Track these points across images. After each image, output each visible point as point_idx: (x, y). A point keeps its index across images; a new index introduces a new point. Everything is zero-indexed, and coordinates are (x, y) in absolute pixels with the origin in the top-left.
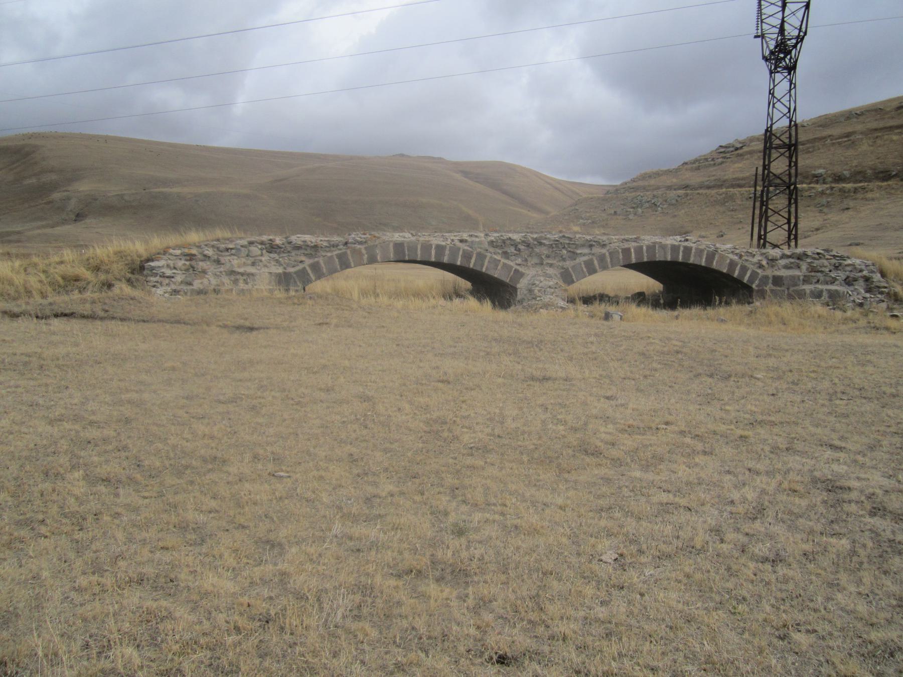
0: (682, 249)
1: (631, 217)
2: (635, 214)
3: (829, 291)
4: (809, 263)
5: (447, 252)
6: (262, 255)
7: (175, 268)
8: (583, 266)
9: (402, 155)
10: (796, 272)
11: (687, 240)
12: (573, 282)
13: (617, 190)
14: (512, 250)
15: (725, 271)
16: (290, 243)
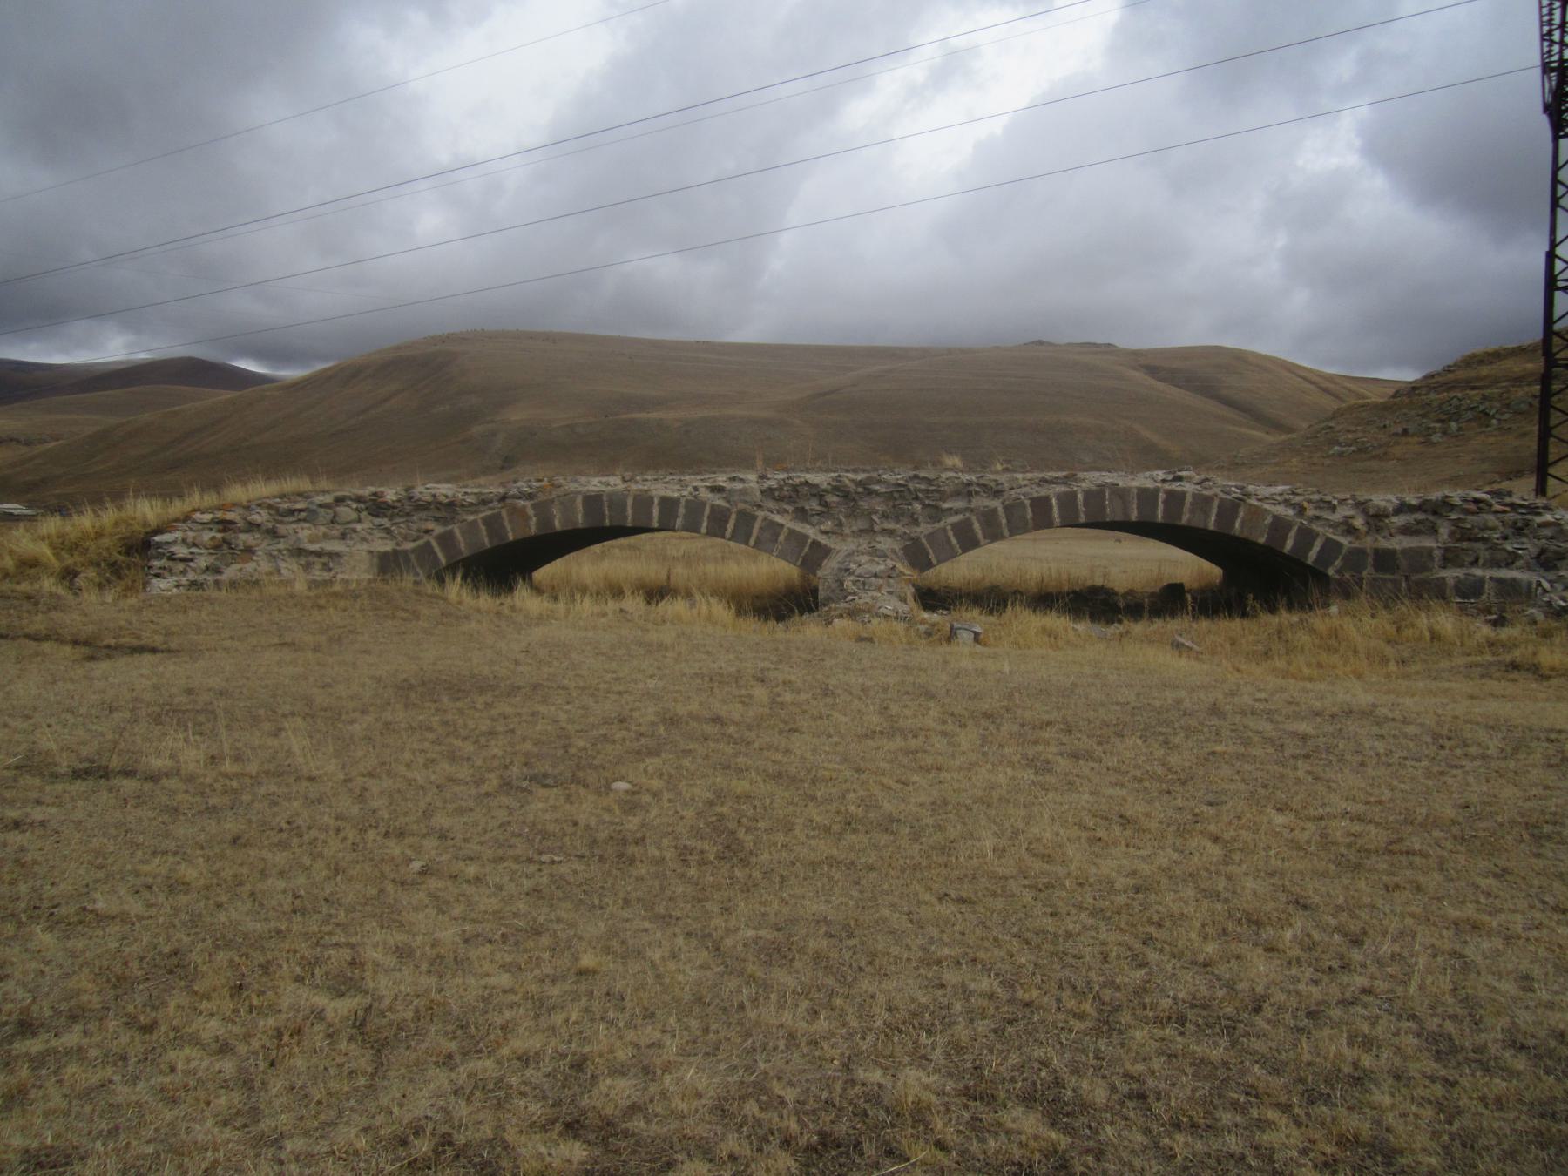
0: (1162, 496)
1: (1435, 438)
2: (1445, 433)
3: (1500, 581)
4: (1456, 522)
5: (682, 511)
6: (359, 521)
7: (194, 545)
8: (950, 533)
9: (1041, 343)
10: (1428, 542)
11: (1180, 479)
12: (930, 565)
13: (1413, 388)
14: (814, 505)
15: (1262, 540)
16: (410, 498)
